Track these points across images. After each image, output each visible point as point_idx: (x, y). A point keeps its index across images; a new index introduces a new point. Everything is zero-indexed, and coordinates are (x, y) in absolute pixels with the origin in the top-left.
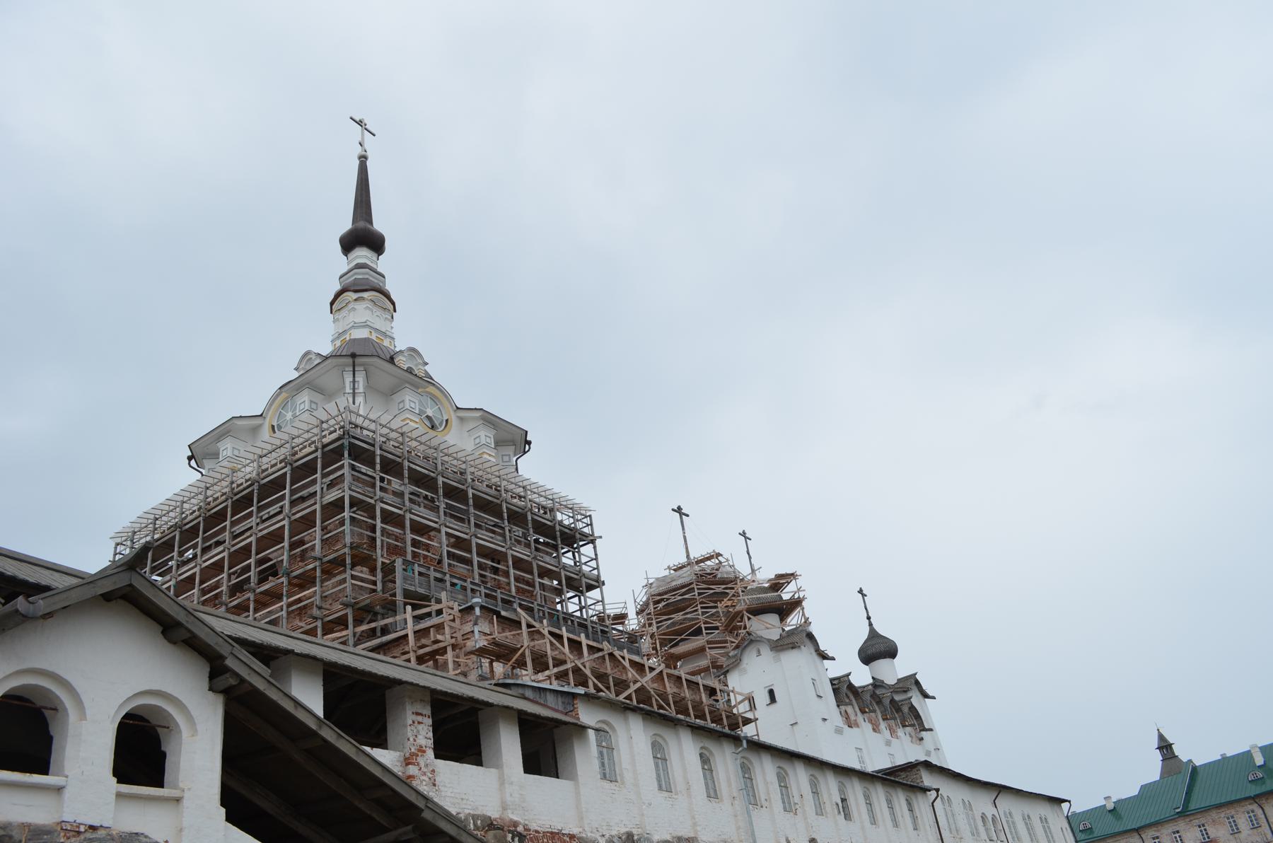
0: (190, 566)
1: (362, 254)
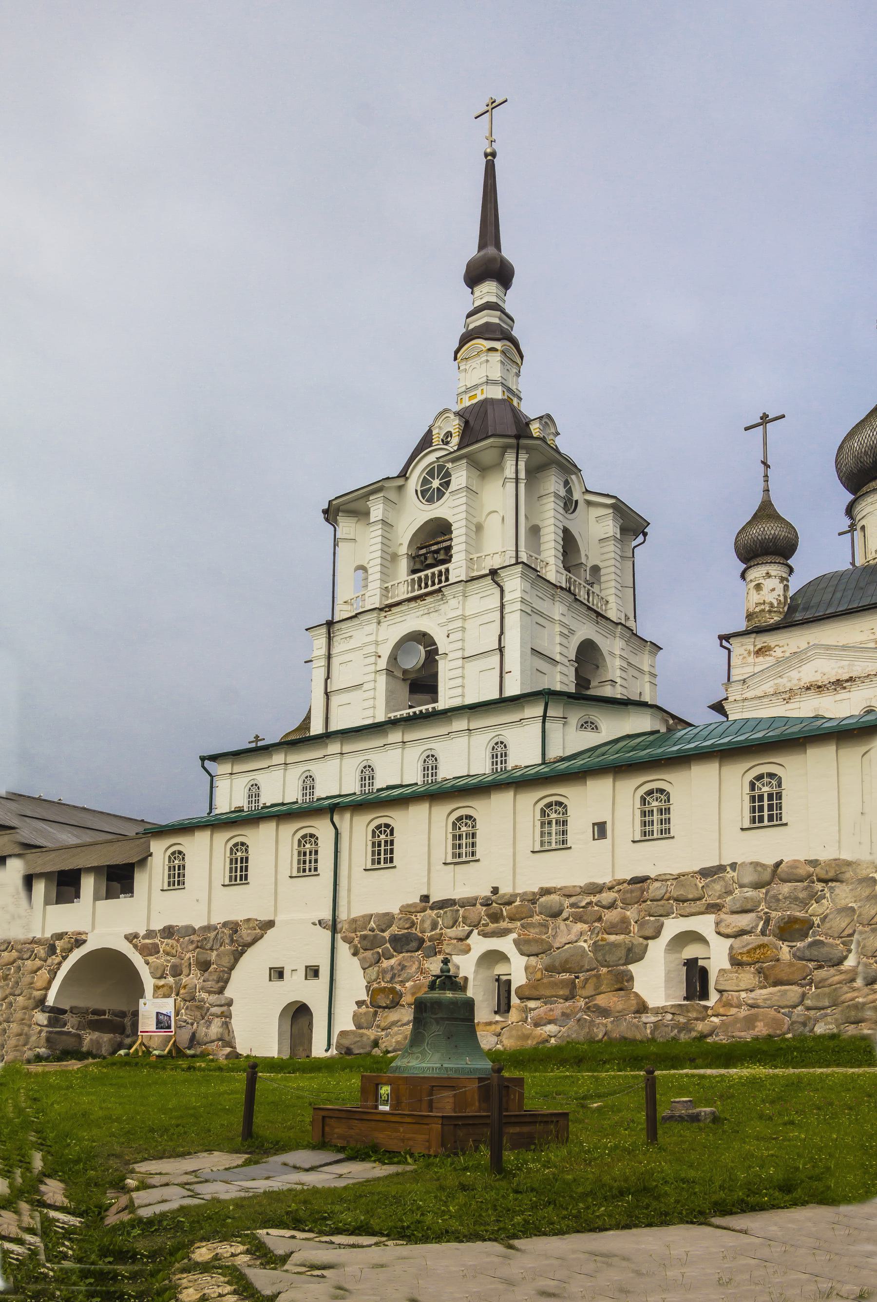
1: (488, 291)
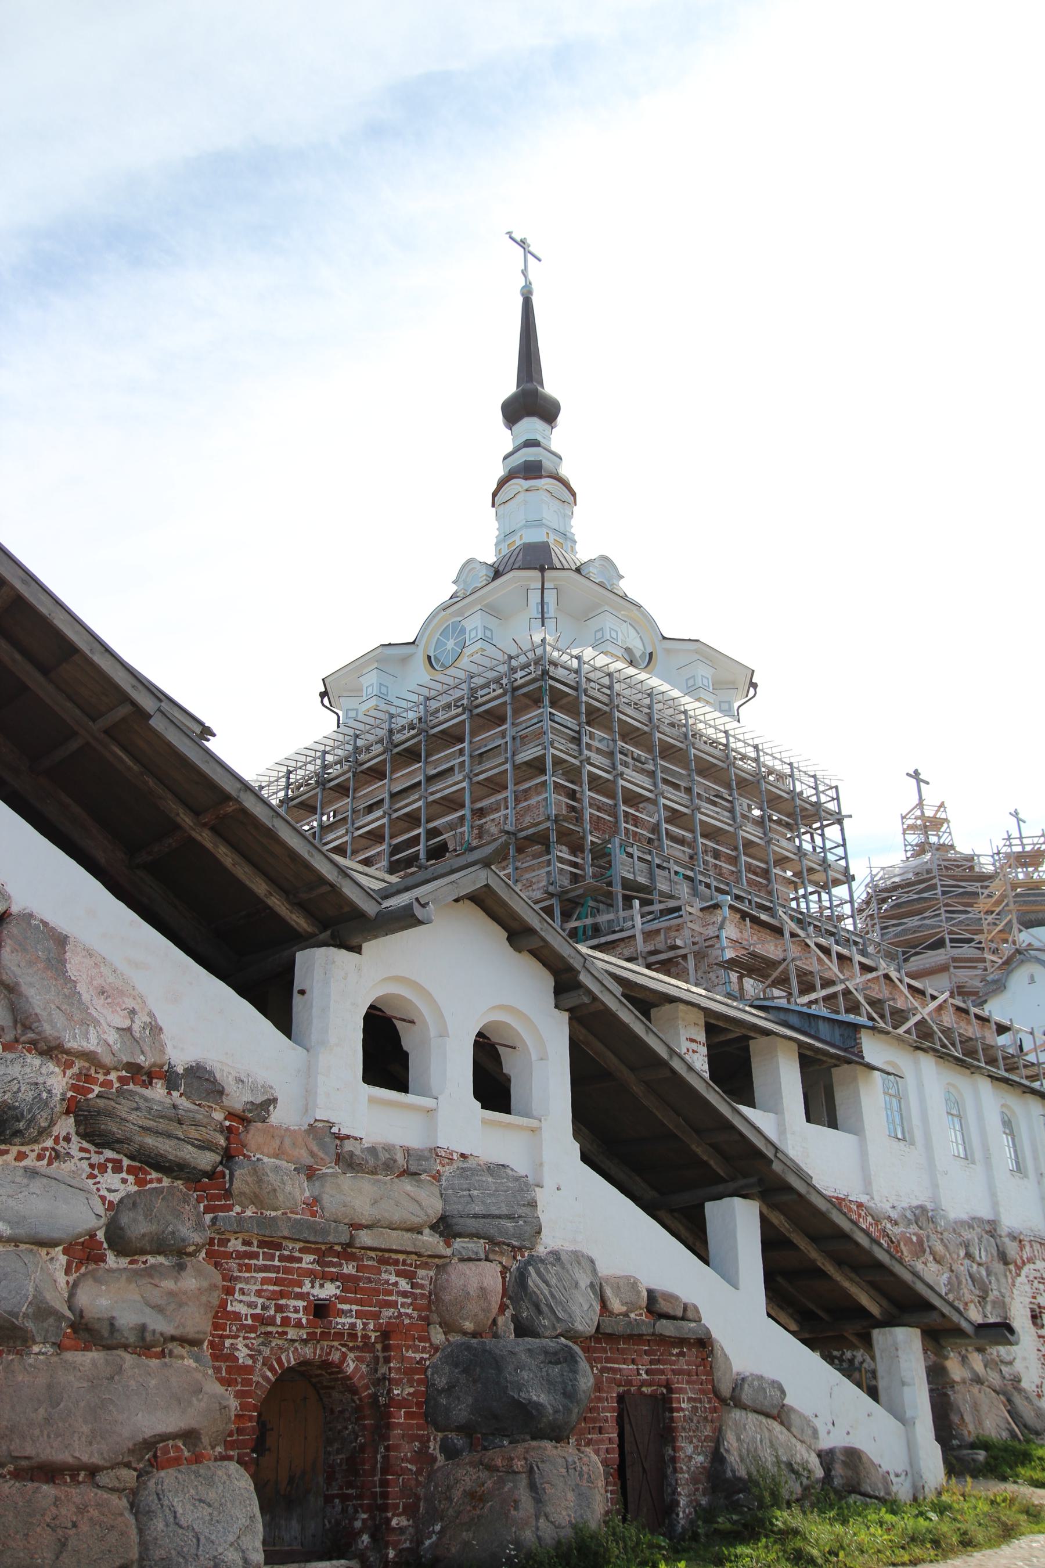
0: (339, 834)
1: (530, 426)
